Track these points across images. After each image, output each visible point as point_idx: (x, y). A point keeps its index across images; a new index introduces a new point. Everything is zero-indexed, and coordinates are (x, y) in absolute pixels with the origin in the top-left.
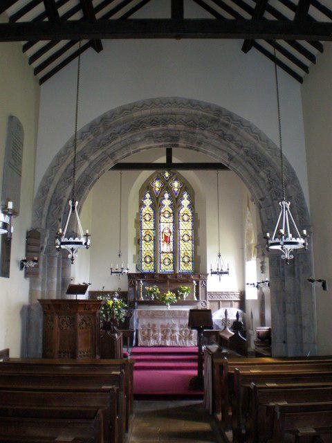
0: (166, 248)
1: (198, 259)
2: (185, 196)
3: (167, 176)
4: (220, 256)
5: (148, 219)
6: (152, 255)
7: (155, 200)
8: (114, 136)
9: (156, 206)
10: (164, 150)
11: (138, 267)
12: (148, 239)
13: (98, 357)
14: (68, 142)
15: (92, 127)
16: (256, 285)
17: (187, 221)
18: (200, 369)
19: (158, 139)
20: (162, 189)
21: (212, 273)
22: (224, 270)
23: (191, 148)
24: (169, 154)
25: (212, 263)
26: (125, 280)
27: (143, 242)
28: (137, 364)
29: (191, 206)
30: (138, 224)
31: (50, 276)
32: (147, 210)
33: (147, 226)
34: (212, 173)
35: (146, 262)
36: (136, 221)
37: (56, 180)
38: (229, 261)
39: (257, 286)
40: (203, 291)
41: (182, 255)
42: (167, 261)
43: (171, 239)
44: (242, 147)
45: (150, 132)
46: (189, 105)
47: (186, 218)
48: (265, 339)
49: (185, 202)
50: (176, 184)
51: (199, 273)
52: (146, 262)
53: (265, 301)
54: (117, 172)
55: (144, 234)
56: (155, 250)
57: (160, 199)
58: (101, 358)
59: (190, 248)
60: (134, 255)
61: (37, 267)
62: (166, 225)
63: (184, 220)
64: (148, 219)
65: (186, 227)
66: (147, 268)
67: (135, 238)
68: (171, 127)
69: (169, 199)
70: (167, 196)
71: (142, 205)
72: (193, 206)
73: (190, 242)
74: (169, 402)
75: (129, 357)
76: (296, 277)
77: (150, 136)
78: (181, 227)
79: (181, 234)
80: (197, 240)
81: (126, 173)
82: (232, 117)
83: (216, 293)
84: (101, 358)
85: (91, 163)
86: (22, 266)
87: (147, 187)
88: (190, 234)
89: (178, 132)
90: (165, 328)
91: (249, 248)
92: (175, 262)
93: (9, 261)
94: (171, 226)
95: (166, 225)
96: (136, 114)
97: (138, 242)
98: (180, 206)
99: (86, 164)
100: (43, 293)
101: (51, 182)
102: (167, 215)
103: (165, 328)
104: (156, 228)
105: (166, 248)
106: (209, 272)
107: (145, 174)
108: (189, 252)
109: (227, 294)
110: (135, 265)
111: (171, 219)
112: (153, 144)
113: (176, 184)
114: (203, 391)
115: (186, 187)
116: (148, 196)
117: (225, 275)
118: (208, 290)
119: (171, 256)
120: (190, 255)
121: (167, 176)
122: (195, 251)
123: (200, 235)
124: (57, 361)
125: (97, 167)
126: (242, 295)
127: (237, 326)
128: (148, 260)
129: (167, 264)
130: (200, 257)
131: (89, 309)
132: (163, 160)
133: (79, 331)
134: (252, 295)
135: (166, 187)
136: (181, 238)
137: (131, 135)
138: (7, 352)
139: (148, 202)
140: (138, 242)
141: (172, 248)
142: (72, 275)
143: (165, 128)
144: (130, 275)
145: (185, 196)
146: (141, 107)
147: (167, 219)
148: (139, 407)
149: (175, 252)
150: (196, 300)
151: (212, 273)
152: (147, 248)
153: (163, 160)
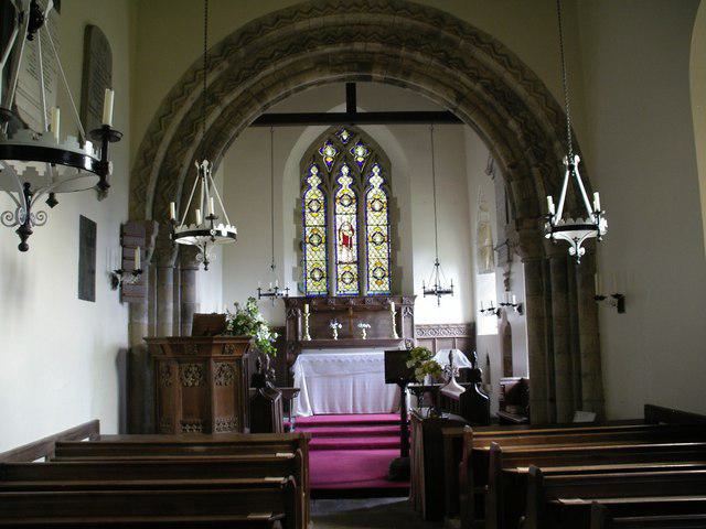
0: (345, 255)
1: (398, 275)
2: (376, 170)
3: (345, 137)
4: (437, 265)
5: (315, 208)
6: (324, 267)
7: (327, 177)
8: (262, 63)
9: (329, 186)
10: (342, 87)
11: (302, 286)
12: (315, 242)
13: (247, 430)
14: (186, 74)
15: (226, 48)
16: (496, 311)
17: (380, 210)
18: (404, 446)
19: (338, 68)
20: (336, 159)
21: (425, 293)
22: (446, 287)
23: (392, 82)
24: (351, 103)
25: (422, 275)
26: (280, 305)
27: (308, 246)
28: (313, 441)
29: (386, 186)
30: (300, 217)
31: (162, 300)
32: (313, 194)
33: (315, 220)
34: (420, 130)
35: (314, 279)
36: (296, 213)
37: (168, 138)
38: (450, 276)
39: (498, 313)
40: (409, 324)
41: (372, 267)
42: (347, 276)
43: (354, 241)
44: (478, 78)
45: (323, 56)
46: (389, 7)
47: (377, 206)
48: (516, 396)
49: (376, 180)
50: (360, 151)
51: (400, 289)
52: (314, 279)
53: (513, 336)
54: (265, 130)
55: (308, 234)
56: (328, 260)
57: (334, 176)
58: (252, 432)
59: (385, 255)
60: (294, 269)
61: (139, 283)
62: (345, 217)
63: (374, 210)
64: (315, 208)
65: (377, 220)
66: (315, 288)
67: (295, 241)
68: (358, 46)
69: (349, 175)
70: (345, 170)
71: (305, 186)
72: (390, 187)
73: (385, 244)
74: (364, 501)
75: (292, 430)
76: (570, 293)
77: (323, 63)
78: (370, 221)
79: (371, 232)
80: (394, 240)
81: (281, 131)
82: (461, 27)
83: (429, 327)
84: (252, 432)
85: (225, 109)
86: (114, 282)
87: (312, 157)
88: (385, 232)
89: (370, 56)
90: (337, 386)
91: (482, 252)
92: (360, 279)
93: (93, 272)
94: (354, 219)
95: (345, 217)
96: (301, 25)
97: (301, 246)
98: (368, 186)
99: (218, 111)
100: (150, 327)
101: (159, 141)
102: (346, 202)
103: (337, 386)
104: (329, 222)
105: (345, 255)
106: (418, 290)
107: (312, 132)
108: (383, 262)
109: (447, 327)
110: (296, 284)
111: (353, 209)
112: (328, 77)
113: (360, 151)
114: (408, 480)
115: (376, 155)
116: (314, 170)
117: (449, 295)
118: (416, 322)
119: (354, 268)
120: (386, 267)
121: (345, 137)
122: (391, 260)
123: (401, 233)
124: (179, 438)
125: (234, 114)
126: (471, 329)
127: (469, 376)
128: (317, 275)
129: (347, 281)
130: (401, 268)
131: (231, 351)
132: (342, 109)
133: (215, 388)
134: (488, 327)
135: (344, 156)
136: (370, 239)
137: (291, 60)
138: (95, 425)
139: (314, 181)
140: (301, 246)
141: (355, 255)
142: (197, 302)
143: (348, 48)
144: (287, 301)
145: (376, 170)
146: (308, 13)
147: (346, 209)
148: (318, 507)
149: (361, 261)
150: (397, 337)
151: (425, 293)
152: (315, 256)
153: (342, 109)
